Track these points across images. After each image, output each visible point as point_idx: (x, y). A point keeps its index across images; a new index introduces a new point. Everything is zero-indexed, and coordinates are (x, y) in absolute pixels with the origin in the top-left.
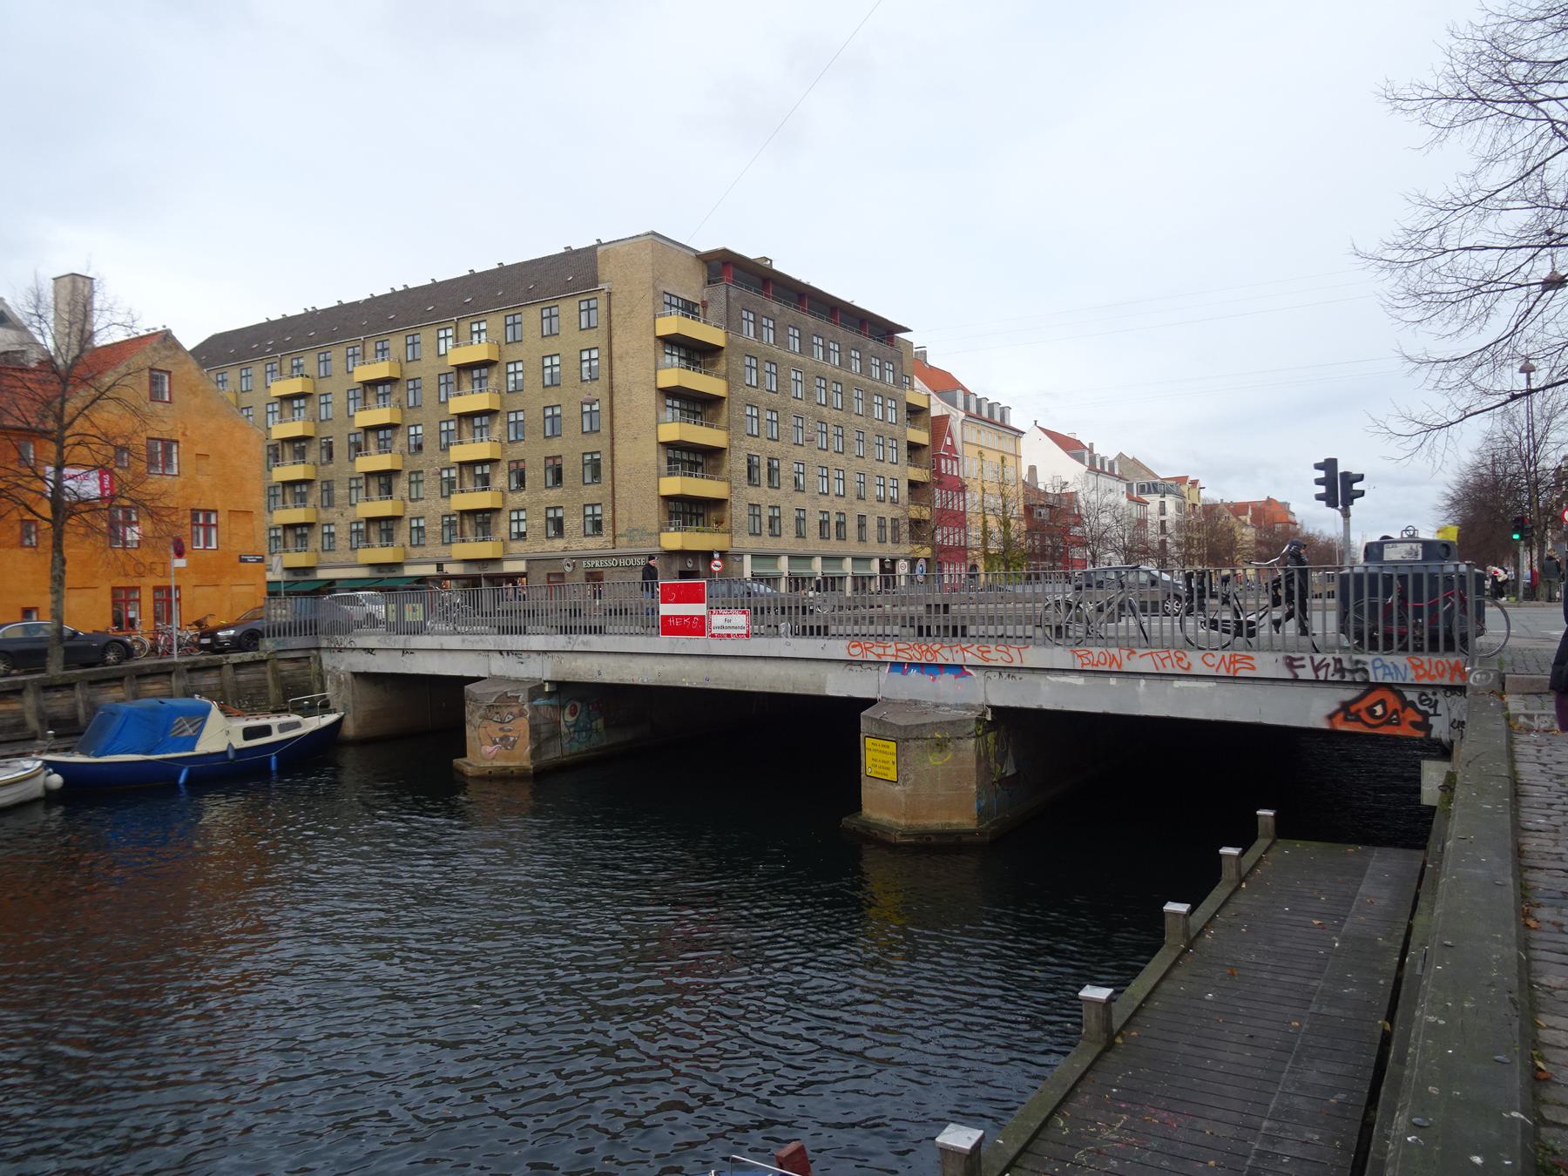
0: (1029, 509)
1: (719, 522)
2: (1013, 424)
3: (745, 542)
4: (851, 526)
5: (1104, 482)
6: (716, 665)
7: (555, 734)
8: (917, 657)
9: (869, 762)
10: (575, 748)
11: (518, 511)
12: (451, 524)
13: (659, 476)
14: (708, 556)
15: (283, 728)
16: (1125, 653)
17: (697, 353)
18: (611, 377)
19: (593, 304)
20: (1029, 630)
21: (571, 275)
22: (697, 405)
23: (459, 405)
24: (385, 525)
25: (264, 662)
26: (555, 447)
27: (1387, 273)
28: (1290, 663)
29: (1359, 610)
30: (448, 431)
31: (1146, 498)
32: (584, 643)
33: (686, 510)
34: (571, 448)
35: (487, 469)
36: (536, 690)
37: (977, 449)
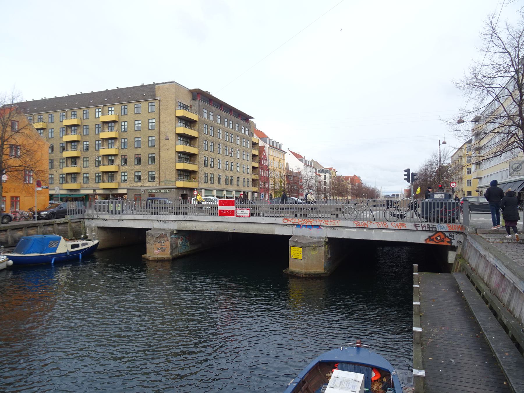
0: (287, 177)
1: (194, 178)
2: (283, 150)
3: (203, 185)
4: (235, 180)
5: (309, 169)
6: (237, 225)
7: (177, 247)
8: (305, 223)
9: (292, 254)
10: (182, 251)
11: (124, 172)
12: (99, 176)
13: (176, 163)
14: (192, 190)
15: (83, 245)
16: (369, 222)
17: (188, 122)
18: (159, 129)
19: (153, 104)
20: (329, 216)
21: (146, 94)
22: (188, 139)
23: (103, 135)
24: (74, 176)
25: (67, 223)
26: (139, 151)
27: (448, 125)
28: (416, 226)
29: (434, 212)
30: (98, 144)
31: (321, 174)
32: (190, 218)
33: (185, 174)
34: (144, 152)
35: (113, 158)
36: (172, 233)
37: (272, 157)
